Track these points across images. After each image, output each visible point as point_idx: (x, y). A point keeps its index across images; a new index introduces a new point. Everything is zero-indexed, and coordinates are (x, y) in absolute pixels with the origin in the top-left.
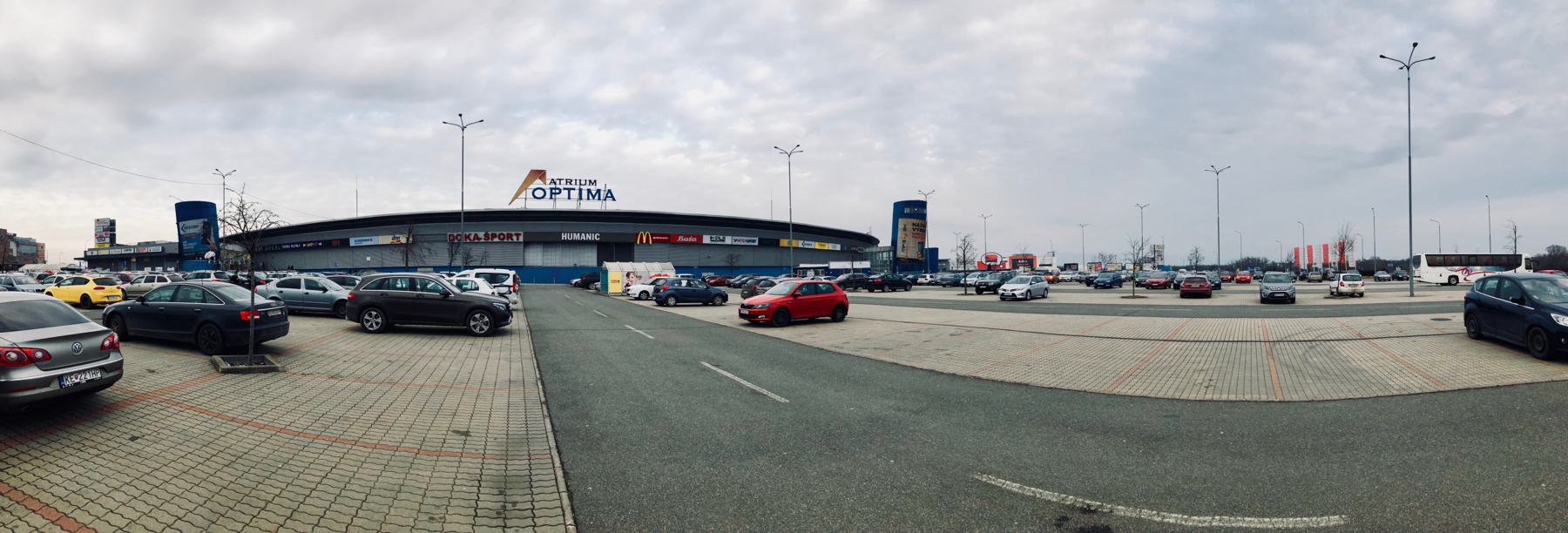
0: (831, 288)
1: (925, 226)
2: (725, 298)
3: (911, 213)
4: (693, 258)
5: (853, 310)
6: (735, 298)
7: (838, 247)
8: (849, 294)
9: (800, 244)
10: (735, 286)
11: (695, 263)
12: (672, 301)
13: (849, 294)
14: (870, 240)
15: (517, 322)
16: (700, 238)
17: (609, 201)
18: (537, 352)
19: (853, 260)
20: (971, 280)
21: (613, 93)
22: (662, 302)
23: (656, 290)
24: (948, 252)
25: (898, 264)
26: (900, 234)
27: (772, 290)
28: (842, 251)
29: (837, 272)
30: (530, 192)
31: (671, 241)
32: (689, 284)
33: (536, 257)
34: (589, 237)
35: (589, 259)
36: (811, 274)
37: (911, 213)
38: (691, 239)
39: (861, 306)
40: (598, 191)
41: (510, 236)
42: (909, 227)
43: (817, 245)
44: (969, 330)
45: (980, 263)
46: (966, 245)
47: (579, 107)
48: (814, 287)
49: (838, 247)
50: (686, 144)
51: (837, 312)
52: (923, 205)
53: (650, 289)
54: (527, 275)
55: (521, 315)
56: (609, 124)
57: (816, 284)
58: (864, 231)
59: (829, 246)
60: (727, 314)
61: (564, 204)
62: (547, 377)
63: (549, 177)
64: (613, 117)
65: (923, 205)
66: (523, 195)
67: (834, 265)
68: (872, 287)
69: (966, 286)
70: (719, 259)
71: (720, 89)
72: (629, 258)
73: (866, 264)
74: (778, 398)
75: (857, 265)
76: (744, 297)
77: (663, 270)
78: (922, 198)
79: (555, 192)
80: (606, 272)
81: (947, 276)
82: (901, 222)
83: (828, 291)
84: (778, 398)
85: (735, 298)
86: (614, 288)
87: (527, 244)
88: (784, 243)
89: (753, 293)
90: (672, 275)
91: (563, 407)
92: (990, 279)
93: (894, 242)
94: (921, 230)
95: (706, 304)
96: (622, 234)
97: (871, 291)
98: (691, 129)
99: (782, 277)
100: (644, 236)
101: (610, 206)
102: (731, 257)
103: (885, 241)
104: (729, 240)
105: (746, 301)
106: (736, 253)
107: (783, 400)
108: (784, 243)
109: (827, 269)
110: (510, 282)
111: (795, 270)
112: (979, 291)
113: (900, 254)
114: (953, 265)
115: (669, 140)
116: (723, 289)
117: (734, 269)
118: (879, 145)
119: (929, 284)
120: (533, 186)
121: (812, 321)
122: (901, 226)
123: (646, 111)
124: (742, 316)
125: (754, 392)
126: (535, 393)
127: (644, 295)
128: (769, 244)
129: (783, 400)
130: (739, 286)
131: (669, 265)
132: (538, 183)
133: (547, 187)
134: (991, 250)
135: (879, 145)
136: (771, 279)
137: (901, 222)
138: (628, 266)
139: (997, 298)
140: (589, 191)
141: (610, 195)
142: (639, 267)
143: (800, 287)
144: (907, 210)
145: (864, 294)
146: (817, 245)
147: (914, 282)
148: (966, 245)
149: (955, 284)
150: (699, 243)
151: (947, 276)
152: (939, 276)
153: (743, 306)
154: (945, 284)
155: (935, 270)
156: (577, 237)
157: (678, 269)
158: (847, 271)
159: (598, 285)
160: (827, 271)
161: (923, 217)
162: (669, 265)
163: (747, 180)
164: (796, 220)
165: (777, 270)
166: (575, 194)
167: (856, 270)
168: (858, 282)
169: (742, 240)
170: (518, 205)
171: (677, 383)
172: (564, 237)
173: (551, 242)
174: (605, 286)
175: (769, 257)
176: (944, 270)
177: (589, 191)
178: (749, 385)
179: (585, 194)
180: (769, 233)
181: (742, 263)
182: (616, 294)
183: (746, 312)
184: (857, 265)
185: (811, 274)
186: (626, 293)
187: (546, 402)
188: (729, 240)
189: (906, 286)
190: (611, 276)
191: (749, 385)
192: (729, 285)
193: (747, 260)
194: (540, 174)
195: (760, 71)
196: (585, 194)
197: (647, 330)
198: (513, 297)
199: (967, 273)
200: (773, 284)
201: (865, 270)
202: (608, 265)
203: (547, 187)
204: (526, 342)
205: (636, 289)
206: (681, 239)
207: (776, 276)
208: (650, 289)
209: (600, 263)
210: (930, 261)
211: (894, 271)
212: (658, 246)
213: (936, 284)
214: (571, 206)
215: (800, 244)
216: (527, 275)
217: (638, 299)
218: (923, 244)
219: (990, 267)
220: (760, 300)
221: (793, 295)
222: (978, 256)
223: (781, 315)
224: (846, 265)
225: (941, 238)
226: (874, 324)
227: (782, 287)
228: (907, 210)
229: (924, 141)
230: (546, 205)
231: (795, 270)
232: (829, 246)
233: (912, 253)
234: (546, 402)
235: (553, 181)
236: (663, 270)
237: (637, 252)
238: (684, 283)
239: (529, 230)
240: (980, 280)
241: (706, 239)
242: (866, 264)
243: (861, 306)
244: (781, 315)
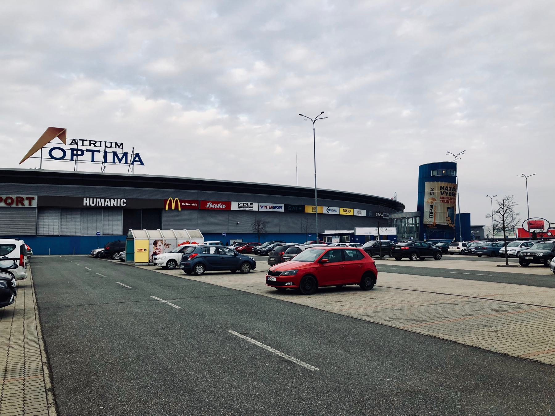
0: (359, 254)
1: (454, 189)
2: (253, 265)
3: (440, 176)
4: (221, 225)
5: (382, 278)
6: (262, 265)
7: (363, 213)
8: (377, 262)
9: (325, 210)
10: (262, 253)
11: (223, 230)
12: (200, 269)
13: (377, 262)
14: (399, 207)
15: (23, 300)
16: (229, 205)
17: (137, 166)
18: (45, 334)
19: (379, 226)
20: (512, 249)
21: (164, 66)
22: (190, 270)
23: (184, 259)
24: (481, 216)
25: (424, 230)
26: (427, 199)
27: (298, 256)
28: (367, 217)
29: (363, 239)
30: (46, 151)
31: (201, 208)
32: (217, 251)
33: (52, 225)
34: (114, 203)
35: (114, 226)
36: (336, 240)
37: (440, 176)
38: (219, 206)
39: (391, 276)
40: (126, 155)
41: (20, 200)
42: (437, 191)
43: (341, 211)
44: (518, 306)
45: (522, 231)
46: (505, 209)
47: (129, 76)
48: (340, 253)
49: (363, 213)
50: (226, 116)
51: (366, 280)
52: (452, 166)
53: (178, 257)
54: (38, 245)
55: (30, 293)
56: (156, 94)
57: (343, 250)
58: (388, 196)
59: (354, 212)
60: (255, 282)
61: (86, 166)
62: (56, 360)
63: (69, 136)
64: (160, 88)
65: (452, 166)
66: (38, 154)
67: (360, 231)
68: (399, 254)
69: (505, 256)
70: (247, 226)
71: (260, 67)
72: (156, 224)
73: (392, 231)
74: (307, 366)
75: (384, 231)
76: (271, 264)
77: (192, 237)
78: (450, 159)
79: (76, 154)
80: (132, 240)
81: (483, 244)
82: (428, 186)
83: (355, 257)
84: (307, 366)
85: (262, 265)
86: (140, 257)
87: (41, 209)
88: (309, 209)
89: (281, 260)
90: (200, 242)
91: (73, 391)
92: (538, 249)
93: (421, 207)
94: (451, 193)
95: (233, 272)
96: (150, 199)
97: (398, 259)
98: (232, 101)
99: (308, 244)
100: (173, 202)
101: (138, 171)
102: (258, 223)
103: (411, 207)
104: (256, 207)
105: (274, 268)
106: (263, 219)
107: (313, 368)
108: (309, 209)
109: (352, 235)
110: (16, 253)
111: (321, 237)
112: (524, 261)
113: (428, 220)
114: (488, 233)
115: (212, 112)
116: (251, 256)
117: (262, 236)
118: (406, 113)
119: (462, 253)
120: (50, 145)
121: (340, 289)
122: (427, 190)
123: (196, 85)
124: (269, 283)
125: (283, 360)
126: (40, 381)
127: (171, 264)
128: (295, 210)
129: (313, 368)
130: (266, 253)
131: (198, 232)
132: (56, 142)
133: (67, 148)
134: (536, 214)
135: (406, 113)
136: (297, 245)
137: (428, 186)
138: (155, 234)
139: (548, 271)
140: (115, 154)
141: (137, 158)
142: (167, 234)
143: (327, 253)
144: (433, 173)
145: (391, 262)
146: (341, 211)
147: (445, 250)
148: (505, 209)
149: (493, 253)
150: (228, 209)
151: (483, 244)
152: (473, 245)
153: (270, 273)
154: (480, 254)
155: (467, 237)
156: (100, 202)
157: (207, 236)
158: (373, 238)
159: (123, 254)
160: (353, 237)
161: (453, 179)
162: (198, 232)
163: (279, 149)
164: (322, 186)
165: (303, 237)
166: (99, 157)
167: (382, 237)
168: (385, 249)
169: (268, 207)
170: (32, 165)
171: (204, 353)
172: (86, 202)
173: (70, 208)
174: (131, 255)
175: (293, 224)
176: (479, 238)
177: (115, 154)
178: (278, 353)
179: (110, 157)
180: (294, 199)
181: (269, 230)
182: (143, 264)
183: (273, 279)
184: (384, 231)
185: (336, 240)
186: (153, 262)
187: (52, 390)
188: (256, 207)
189: (436, 255)
190: (137, 245)
191: (278, 353)
192: (256, 252)
193: (272, 227)
194: (60, 133)
195: (298, 53)
196: (110, 157)
197: (174, 300)
198: (20, 271)
199: (507, 241)
200: (299, 251)
201: (390, 237)
202: (135, 233)
203: (67, 148)
204: (32, 325)
205: (164, 257)
206: (209, 205)
207: (302, 242)
208: (178, 257)
209: (126, 231)
210: (460, 228)
211: (421, 238)
212: (187, 213)
213: (470, 253)
214: (95, 169)
215: (325, 210)
216: (39, 246)
217: (166, 268)
218: (453, 209)
219: (534, 236)
220: (285, 266)
221: (320, 261)
222: (521, 221)
223: (309, 282)
224: (372, 231)
225: (475, 202)
226: (404, 294)
227: (308, 254)
228: (433, 173)
229: (454, 105)
230: (65, 166)
231: (321, 237)
232: (354, 212)
233: (441, 219)
234: (52, 390)
235: (74, 141)
236: (192, 237)
237: (165, 218)
238: (212, 250)
239: (43, 194)
240: (525, 250)
241: (234, 206)
242: (392, 231)
243: (391, 276)
244: (309, 282)
